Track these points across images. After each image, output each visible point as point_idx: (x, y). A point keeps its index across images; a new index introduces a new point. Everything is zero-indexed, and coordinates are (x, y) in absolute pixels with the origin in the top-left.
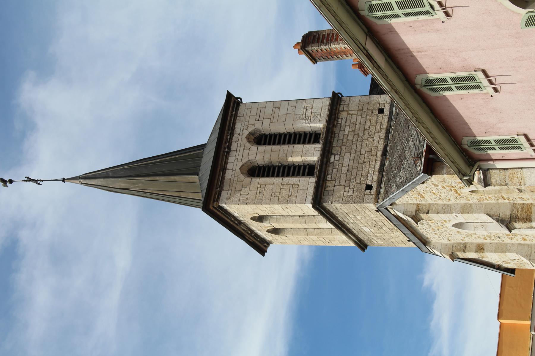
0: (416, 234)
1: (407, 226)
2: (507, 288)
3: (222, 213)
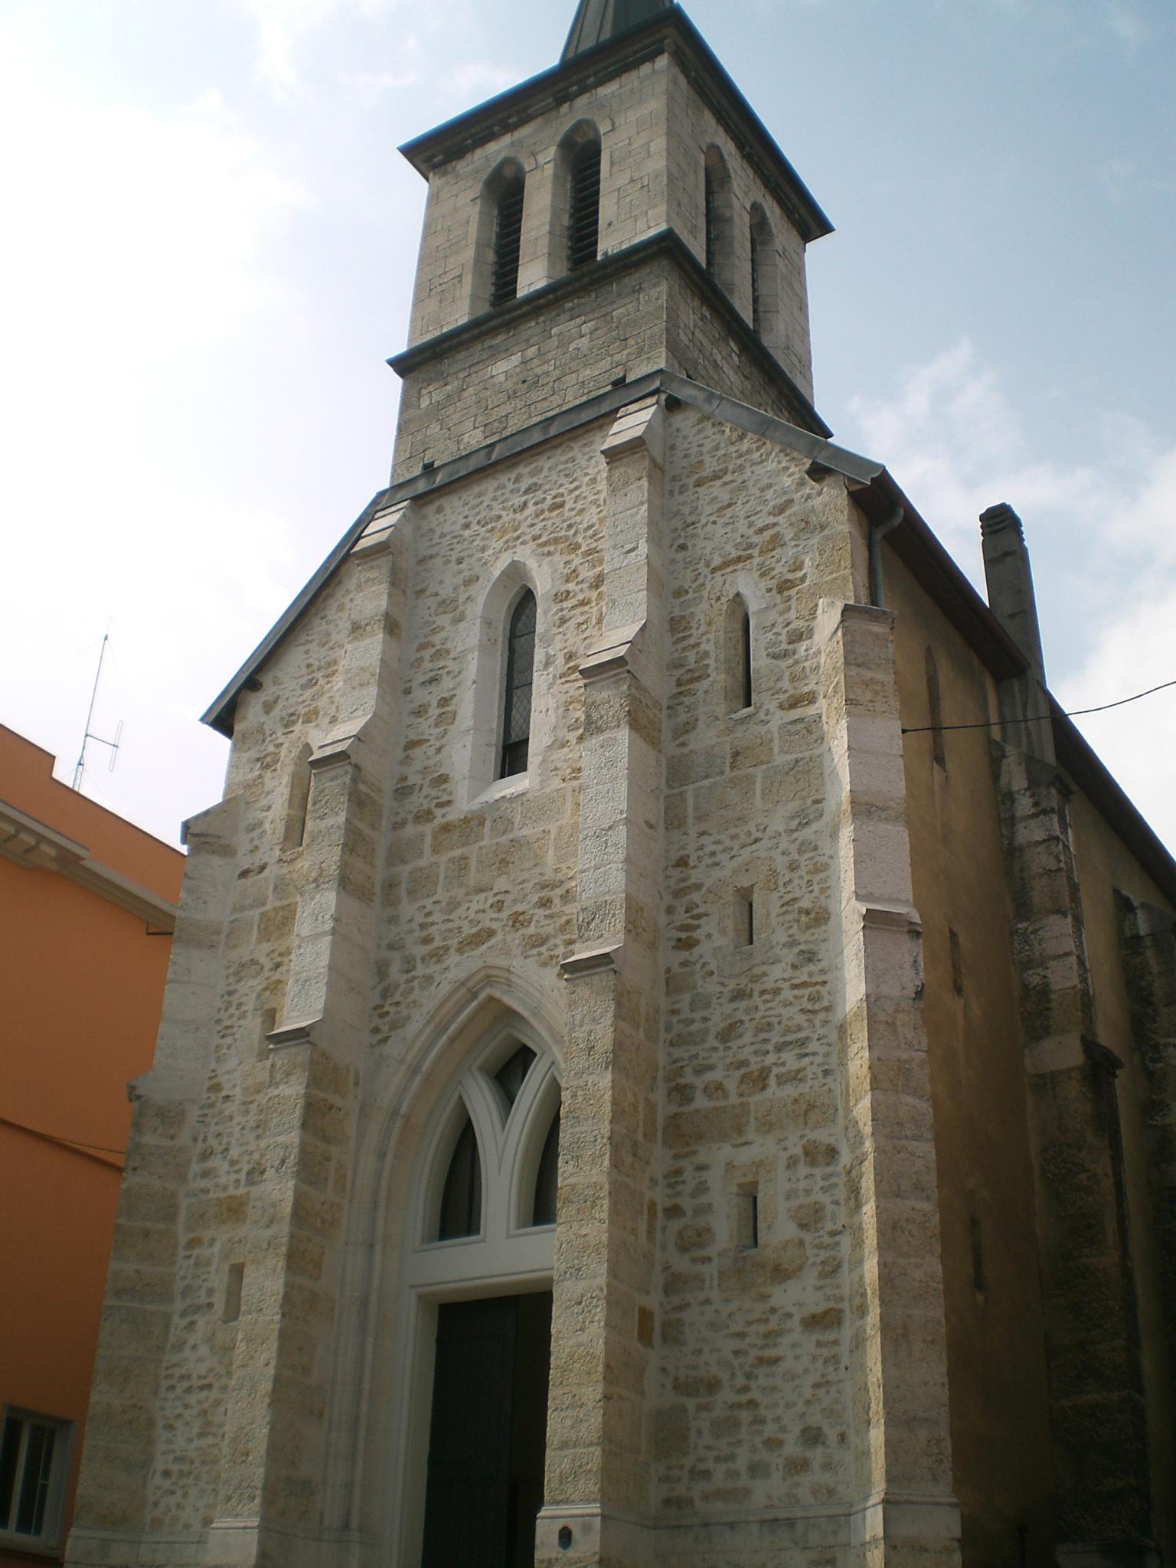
1: (524, 455)
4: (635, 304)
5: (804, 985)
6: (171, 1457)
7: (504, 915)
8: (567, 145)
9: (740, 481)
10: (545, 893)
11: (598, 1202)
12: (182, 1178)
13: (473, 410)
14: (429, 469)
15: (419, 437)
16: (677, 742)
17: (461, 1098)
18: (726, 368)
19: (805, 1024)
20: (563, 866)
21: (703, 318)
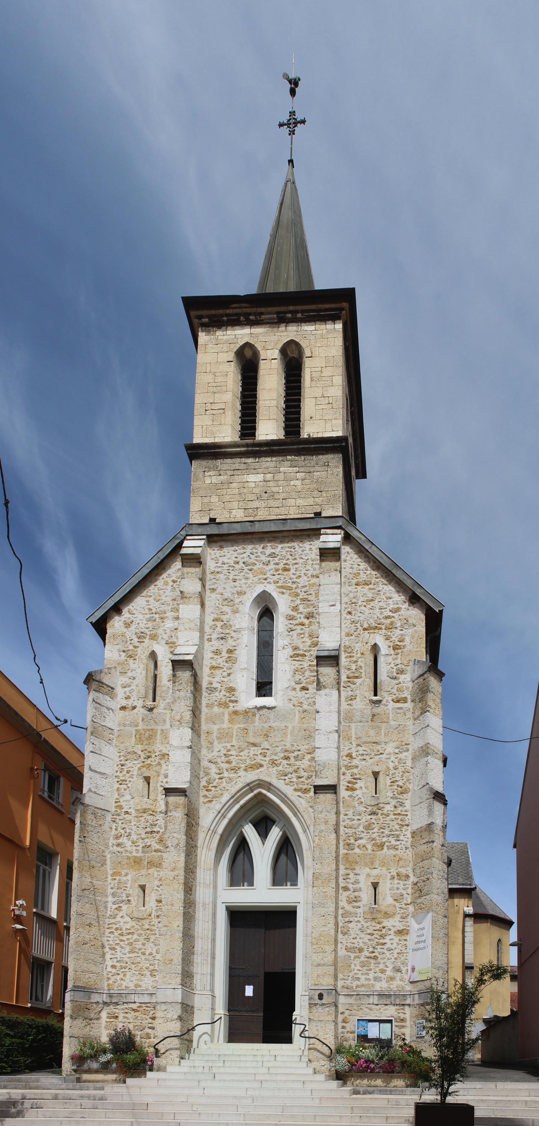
0: (156, 572)
3: (320, 310)
5: (399, 814)
7: (267, 759)
12: (107, 846)
19: (399, 829)
20: (295, 744)
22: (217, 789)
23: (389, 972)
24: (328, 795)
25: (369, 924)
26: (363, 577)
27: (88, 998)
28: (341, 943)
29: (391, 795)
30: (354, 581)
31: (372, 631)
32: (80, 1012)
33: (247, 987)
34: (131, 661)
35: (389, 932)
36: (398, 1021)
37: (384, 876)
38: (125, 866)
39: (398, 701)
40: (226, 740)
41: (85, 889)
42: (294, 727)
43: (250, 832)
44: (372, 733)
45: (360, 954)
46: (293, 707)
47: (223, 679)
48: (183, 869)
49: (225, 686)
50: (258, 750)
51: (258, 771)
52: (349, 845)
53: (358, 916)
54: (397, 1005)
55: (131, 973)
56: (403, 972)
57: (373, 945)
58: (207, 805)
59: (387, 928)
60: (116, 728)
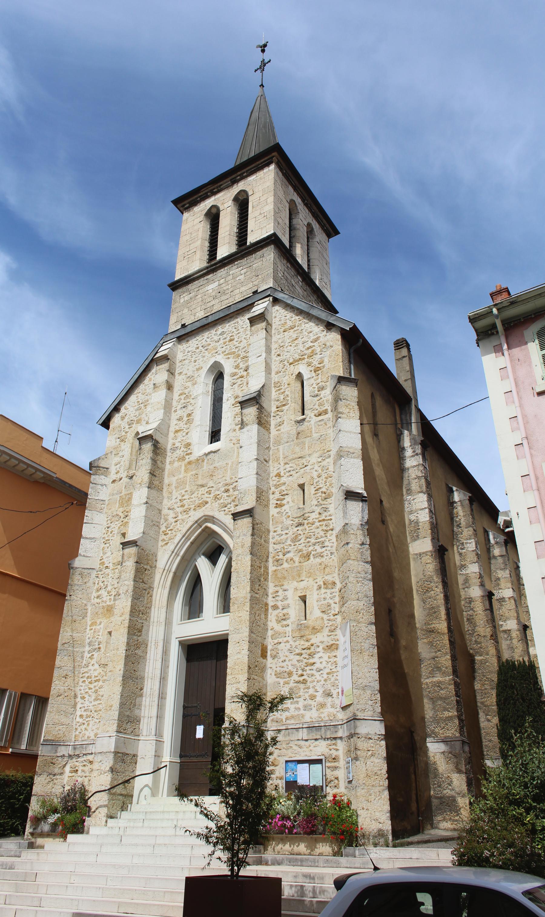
1: (220, 320)
2: (27, 435)
3: (259, 165)
4: (261, 262)
5: (324, 520)
6: (83, 709)
7: (212, 495)
8: (236, 199)
9: (300, 329)
10: (226, 487)
11: (246, 604)
12: (89, 599)
13: (200, 304)
14: (183, 326)
15: (180, 314)
16: (277, 429)
17: (196, 565)
18: (297, 287)
19: (324, 535)
20: (233, 477)
21: (287, 267)
22: (173, 532)
23: (319, 698)
24: (245, 519)
25: (297, 643)
26: (289, 324)
27: (54, 752)
28: (271, 668)
29: (316, 503)
30: (282, 330)
31: (297, 363)
32: (45, 768)
33: (198, 727)
34: (122, 443)
35: (318, 650)
36: (330, 760)
37: (311, 587)
38: (100, 616)
39: (320, 415)
40: (182, 487)
41: (65, 643)
42: (233, 463)
43: (202, 563)
44: (297, 449)
45: (289, 679)
46: (233, 446)
47: (183, 438)
48: (129, 613)
49: (183, 444)
50: (205, 489)
51: (204, 508)
52: (278, 561)
53: (287, 635)
54: (328, 739)
55: (93, 721)
56: (333, 696)
57: (302, 666)
58: (164, 548)
59: (315, 645)
60: (106, 499)
